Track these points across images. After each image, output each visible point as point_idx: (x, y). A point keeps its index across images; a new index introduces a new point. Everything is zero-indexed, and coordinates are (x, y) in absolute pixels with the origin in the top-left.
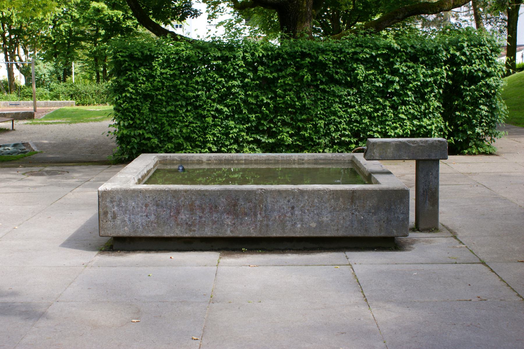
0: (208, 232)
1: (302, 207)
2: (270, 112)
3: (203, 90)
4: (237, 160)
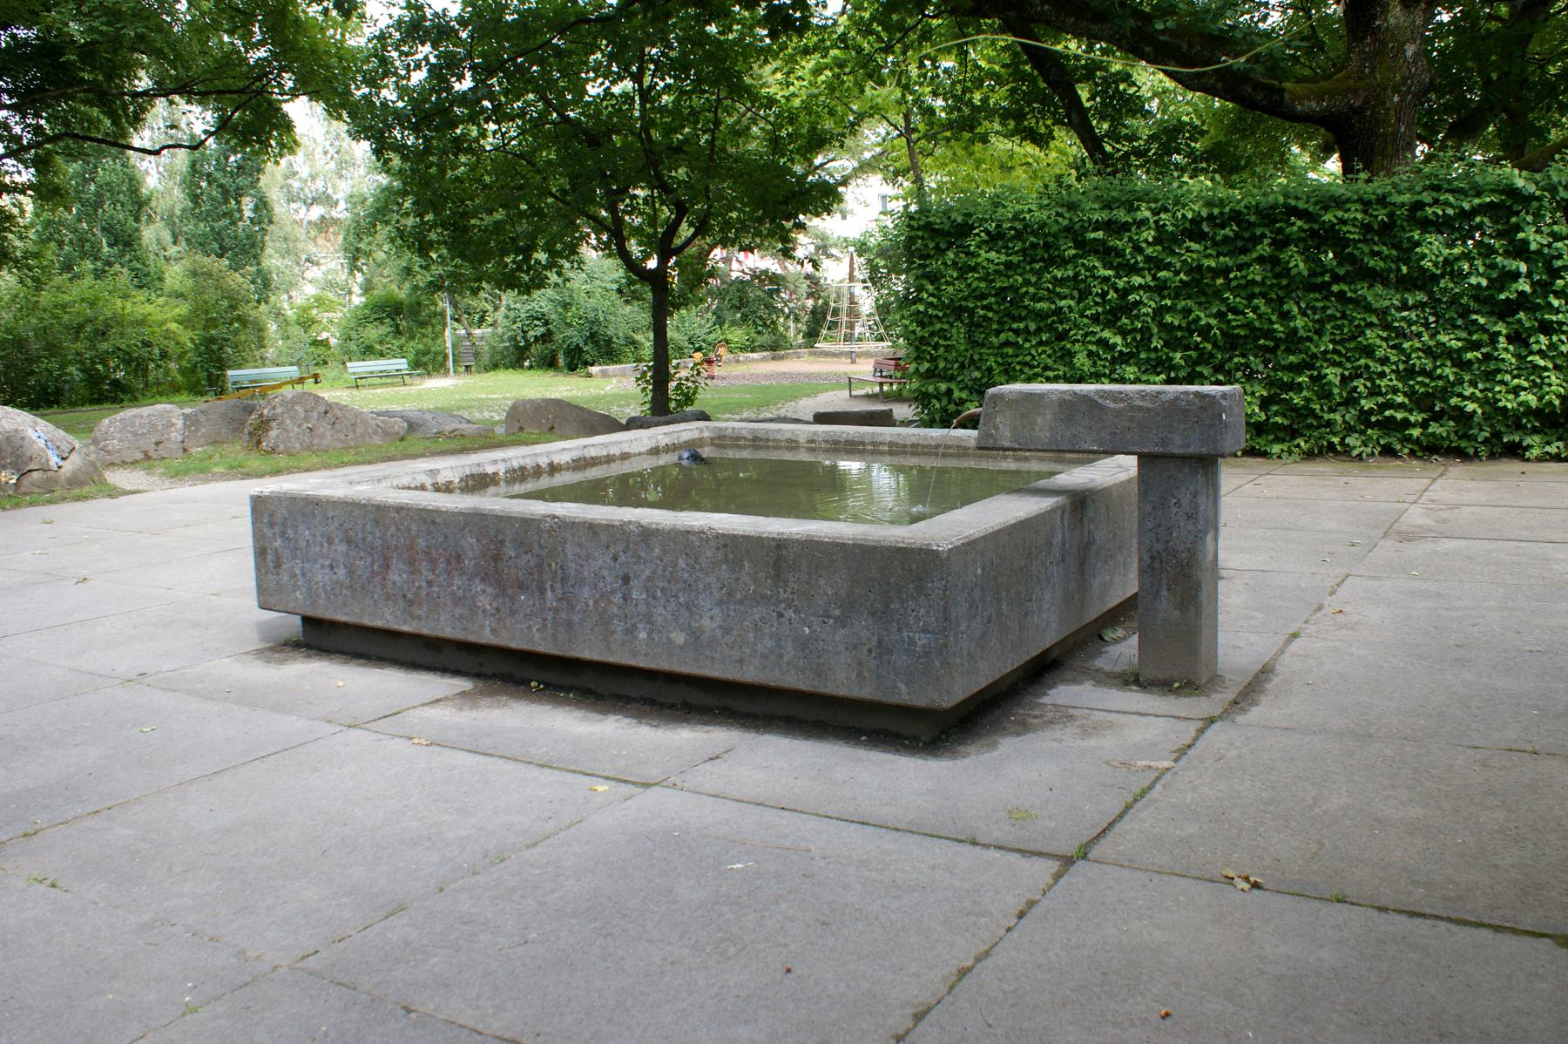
0: (446, 627)
1: (649, 579)
2: (1215, 345)
3: (1072, 298)
4: (873, 443)
